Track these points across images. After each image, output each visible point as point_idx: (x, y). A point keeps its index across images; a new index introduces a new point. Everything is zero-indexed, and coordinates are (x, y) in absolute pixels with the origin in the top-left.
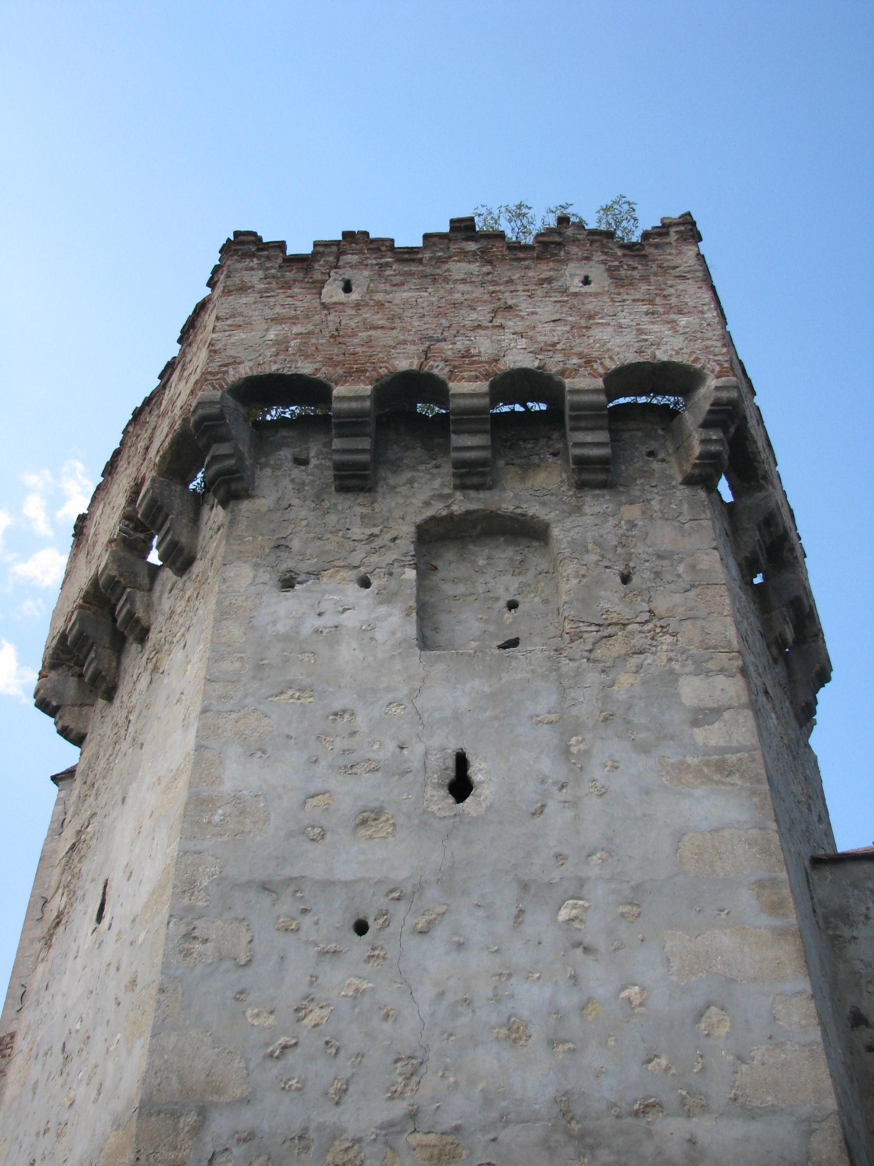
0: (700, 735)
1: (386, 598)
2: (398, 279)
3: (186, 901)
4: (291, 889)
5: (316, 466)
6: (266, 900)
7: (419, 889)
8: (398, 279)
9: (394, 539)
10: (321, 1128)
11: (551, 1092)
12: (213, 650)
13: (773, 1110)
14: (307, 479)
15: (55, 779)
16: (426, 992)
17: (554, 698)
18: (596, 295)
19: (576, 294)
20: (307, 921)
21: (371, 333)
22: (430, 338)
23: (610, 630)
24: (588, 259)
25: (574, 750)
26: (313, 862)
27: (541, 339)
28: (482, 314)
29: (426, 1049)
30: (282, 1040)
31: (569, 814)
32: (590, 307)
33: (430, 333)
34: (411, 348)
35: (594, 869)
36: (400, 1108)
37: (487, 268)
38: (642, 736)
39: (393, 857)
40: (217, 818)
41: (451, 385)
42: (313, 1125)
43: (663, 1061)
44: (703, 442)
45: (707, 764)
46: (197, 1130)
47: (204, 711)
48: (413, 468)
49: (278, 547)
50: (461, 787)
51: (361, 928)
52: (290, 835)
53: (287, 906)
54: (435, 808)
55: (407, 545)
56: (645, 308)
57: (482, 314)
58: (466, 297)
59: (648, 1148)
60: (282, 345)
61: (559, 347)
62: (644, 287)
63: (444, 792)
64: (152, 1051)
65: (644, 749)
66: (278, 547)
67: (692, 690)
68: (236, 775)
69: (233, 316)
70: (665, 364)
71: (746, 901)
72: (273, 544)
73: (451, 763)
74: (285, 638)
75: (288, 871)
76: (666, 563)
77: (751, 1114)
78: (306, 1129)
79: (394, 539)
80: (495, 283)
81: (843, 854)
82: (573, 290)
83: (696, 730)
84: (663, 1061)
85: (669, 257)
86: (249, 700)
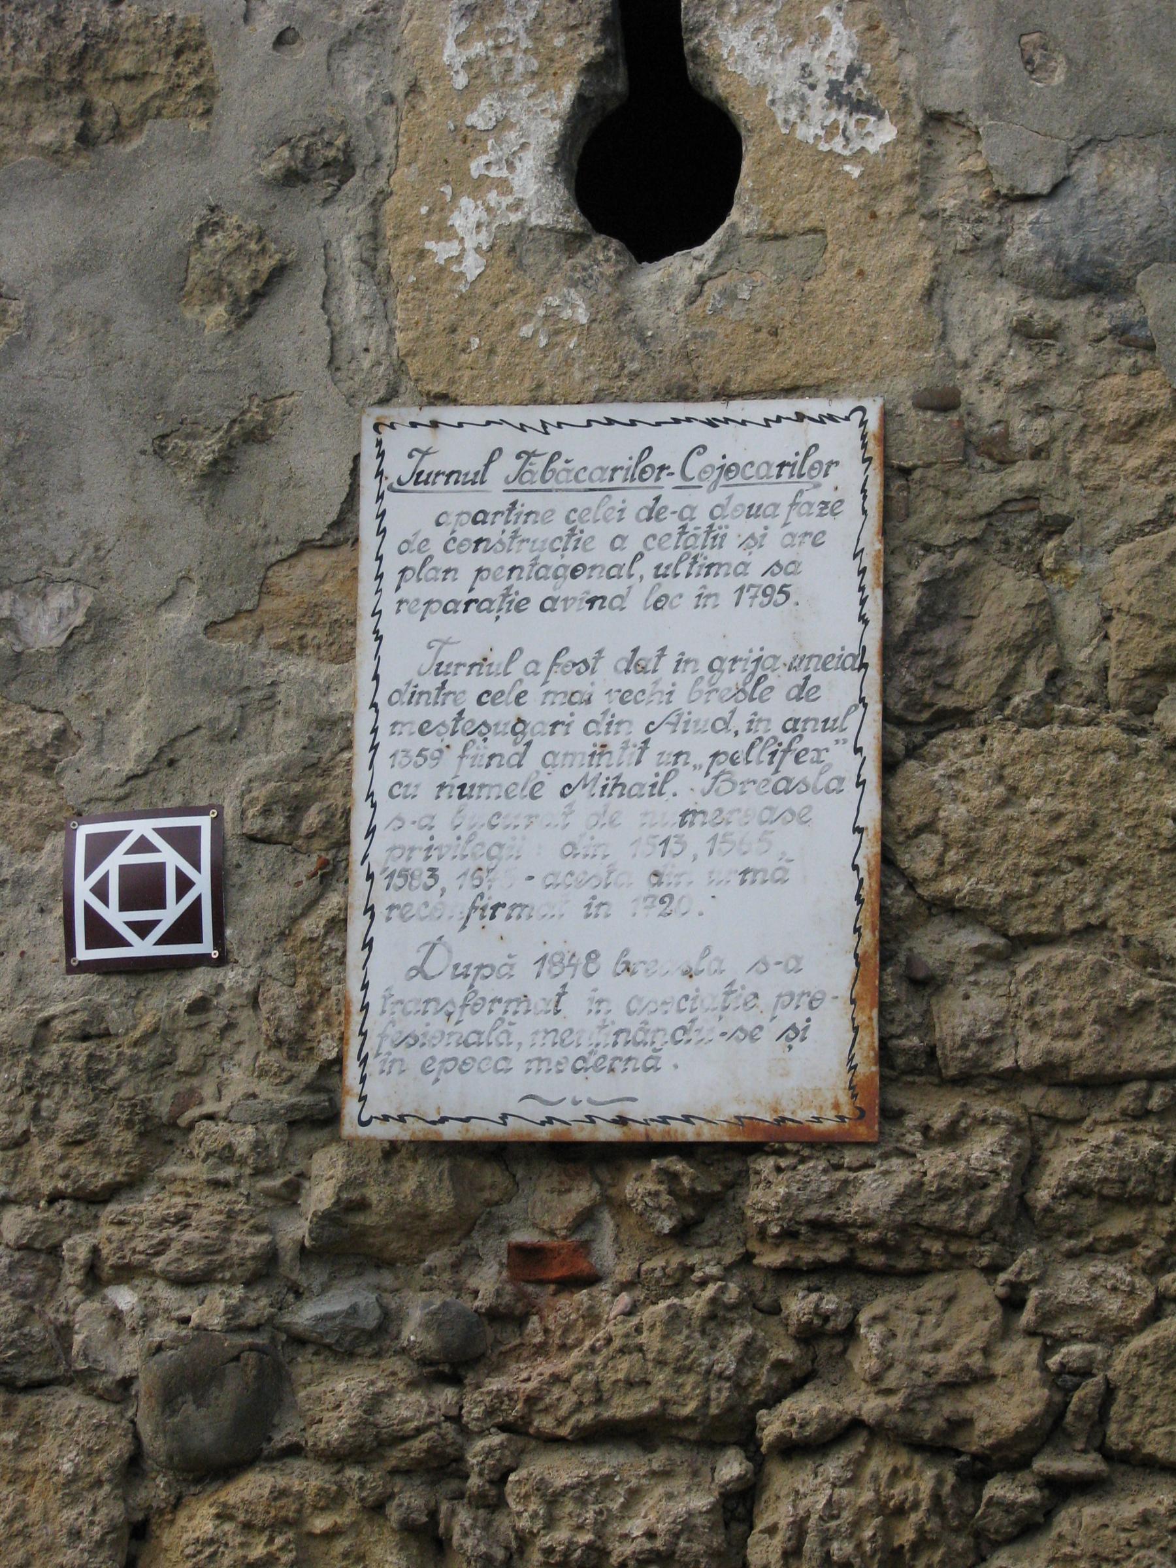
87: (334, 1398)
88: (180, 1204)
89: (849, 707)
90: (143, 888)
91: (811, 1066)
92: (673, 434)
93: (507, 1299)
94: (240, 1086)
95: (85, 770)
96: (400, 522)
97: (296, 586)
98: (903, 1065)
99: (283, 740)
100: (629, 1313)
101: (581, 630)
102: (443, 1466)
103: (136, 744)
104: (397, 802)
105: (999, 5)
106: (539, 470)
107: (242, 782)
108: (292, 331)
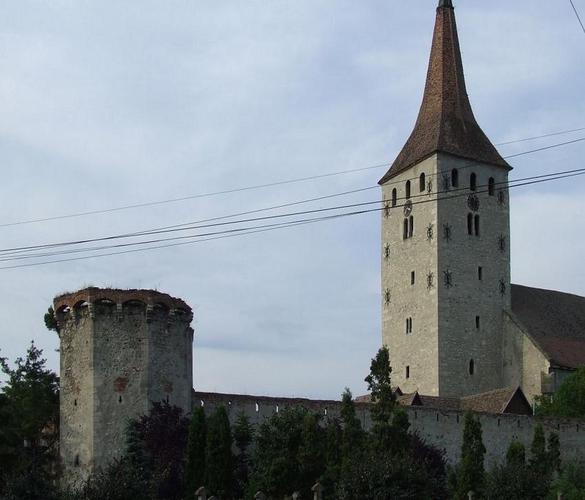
15: (380, 183)
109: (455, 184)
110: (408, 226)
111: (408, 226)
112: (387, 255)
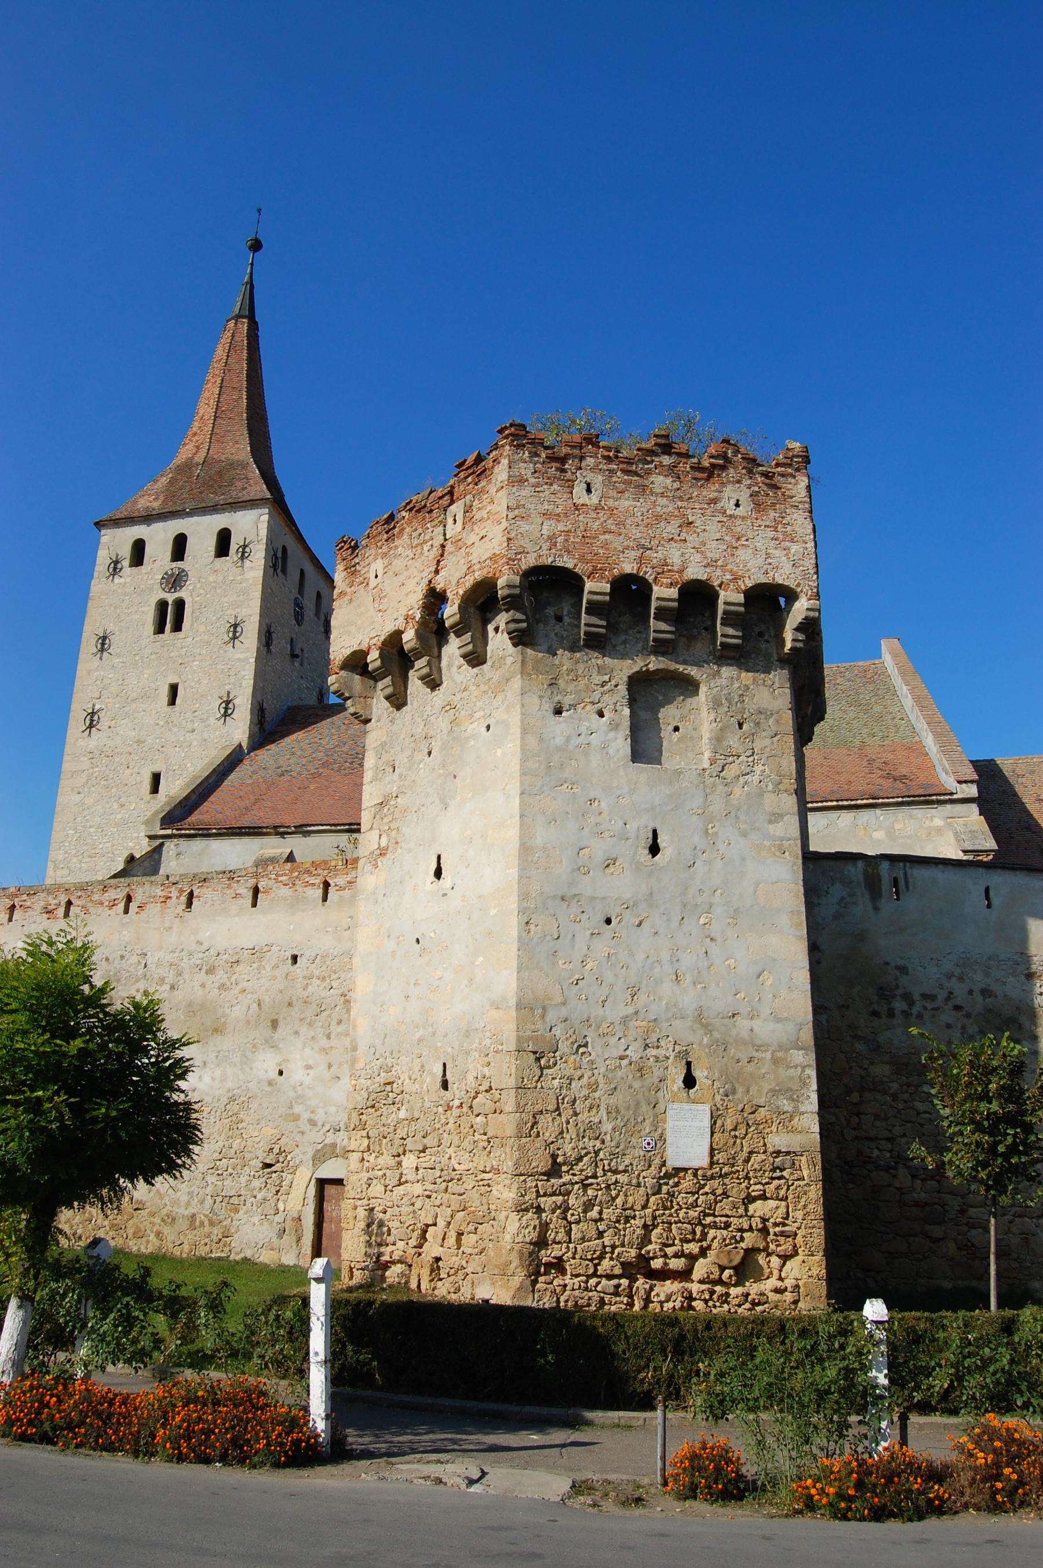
0: (771, 828)
1: (614, 726)
2: (622, 486)
3: (525, 904)
4: (576, 900)
5: (569, 624)
6: (564, 905)
7: (635, 904)
8: (622, 486)
9: (616, 686)
10: (596, 1017)
11: (695, 1006)
12: (523, 754)
13: (787, 1019)
14: (565, 634)
16: (640, 956)
17: (701, 800)
18: (743, 518)
19: (731, 516)
20: (584, 917)
21: (607, 536)
22: (643, 547)
23: (731, 759)
24: (739, 482)
25: (710, 831)
26: (585, 886)
27: (709, 555)
28: (672, 528)
29: (640, 983)
30: (577, 977)
31: (707, 868)
32: (739, 529)
33: (643, 541)
34: (633, 553)
35: (717, 898)
36: (630, 1010)
37: (676, 485)
38: (743, 826)
39: (621, 885)
40: (535, 859)
41: (655, 588)
42: (592, 1015)
43: (742, 995)
44: (794, 640)
45: (774, 846)
46: (543, 1017)
47: (522, 794)
48: (626, 632)
49: (551, 685)
50: (654, 849)
51: (608, 921)
52: (573, 871)
53: (575, 909)
54: (642, 860)
55: (623, 689)
56: (772, 534)
57: (672, 528)
58: (664, 510)
59: (734, 1032)
60: (552, 539)
61: (720, 563)
62: (772, 514)
63: (647, 851)
64: (518, 980)
65: (744, 834)
66: (551, 685)
67: (770, 801)
68: (541, 835)
69: (518, 507)
70: (780, 585)
71: (784, 920)
72: (549, 682)
73: (651, 835)
74: (558, 749)
75: (574, 891)
76: (763, 717)
77: (778, 1020)
78: (589, 1017)
79: (616, 686)
80: (681, 499)
81: (816, 853)
82: (728, 512)
83: (771, 826)
84: (742, 995)
85: (789, 486)
86: (545, 788)
87: (665, 1188)
88: (653, 1171)
89: (708, 1131)
90: (649, 1144)
91: (705, 1162)
92: (694, 1106)
93: (63, 1242)
94: (657, 1161)
95: (643, 1133)
96: (669, 1113)
97: (658, 1120)
98: (712, 1164)
99: (659, 1131)
100: (67, 1237)
101: (686, 1123)
102: (673, 1196)
103: (647, 1131)
104: (669, 1136)
105: (3, 1436)
106: (682, 1109)
107: (656, 1135)
108: (660, 1094)
109: (284, 571)
110: (170, 617)
111: (170, 617)
112: (235, 638)
